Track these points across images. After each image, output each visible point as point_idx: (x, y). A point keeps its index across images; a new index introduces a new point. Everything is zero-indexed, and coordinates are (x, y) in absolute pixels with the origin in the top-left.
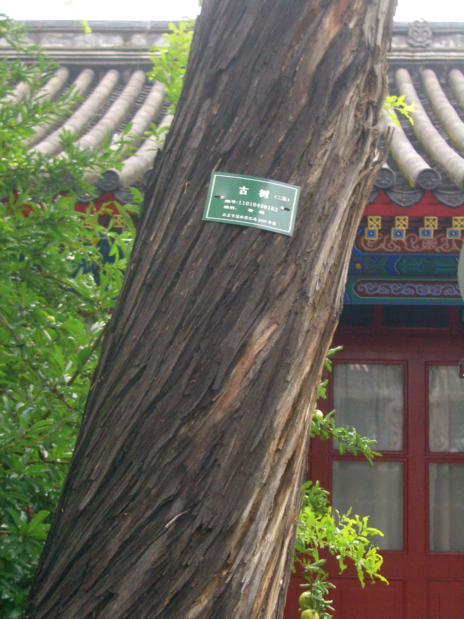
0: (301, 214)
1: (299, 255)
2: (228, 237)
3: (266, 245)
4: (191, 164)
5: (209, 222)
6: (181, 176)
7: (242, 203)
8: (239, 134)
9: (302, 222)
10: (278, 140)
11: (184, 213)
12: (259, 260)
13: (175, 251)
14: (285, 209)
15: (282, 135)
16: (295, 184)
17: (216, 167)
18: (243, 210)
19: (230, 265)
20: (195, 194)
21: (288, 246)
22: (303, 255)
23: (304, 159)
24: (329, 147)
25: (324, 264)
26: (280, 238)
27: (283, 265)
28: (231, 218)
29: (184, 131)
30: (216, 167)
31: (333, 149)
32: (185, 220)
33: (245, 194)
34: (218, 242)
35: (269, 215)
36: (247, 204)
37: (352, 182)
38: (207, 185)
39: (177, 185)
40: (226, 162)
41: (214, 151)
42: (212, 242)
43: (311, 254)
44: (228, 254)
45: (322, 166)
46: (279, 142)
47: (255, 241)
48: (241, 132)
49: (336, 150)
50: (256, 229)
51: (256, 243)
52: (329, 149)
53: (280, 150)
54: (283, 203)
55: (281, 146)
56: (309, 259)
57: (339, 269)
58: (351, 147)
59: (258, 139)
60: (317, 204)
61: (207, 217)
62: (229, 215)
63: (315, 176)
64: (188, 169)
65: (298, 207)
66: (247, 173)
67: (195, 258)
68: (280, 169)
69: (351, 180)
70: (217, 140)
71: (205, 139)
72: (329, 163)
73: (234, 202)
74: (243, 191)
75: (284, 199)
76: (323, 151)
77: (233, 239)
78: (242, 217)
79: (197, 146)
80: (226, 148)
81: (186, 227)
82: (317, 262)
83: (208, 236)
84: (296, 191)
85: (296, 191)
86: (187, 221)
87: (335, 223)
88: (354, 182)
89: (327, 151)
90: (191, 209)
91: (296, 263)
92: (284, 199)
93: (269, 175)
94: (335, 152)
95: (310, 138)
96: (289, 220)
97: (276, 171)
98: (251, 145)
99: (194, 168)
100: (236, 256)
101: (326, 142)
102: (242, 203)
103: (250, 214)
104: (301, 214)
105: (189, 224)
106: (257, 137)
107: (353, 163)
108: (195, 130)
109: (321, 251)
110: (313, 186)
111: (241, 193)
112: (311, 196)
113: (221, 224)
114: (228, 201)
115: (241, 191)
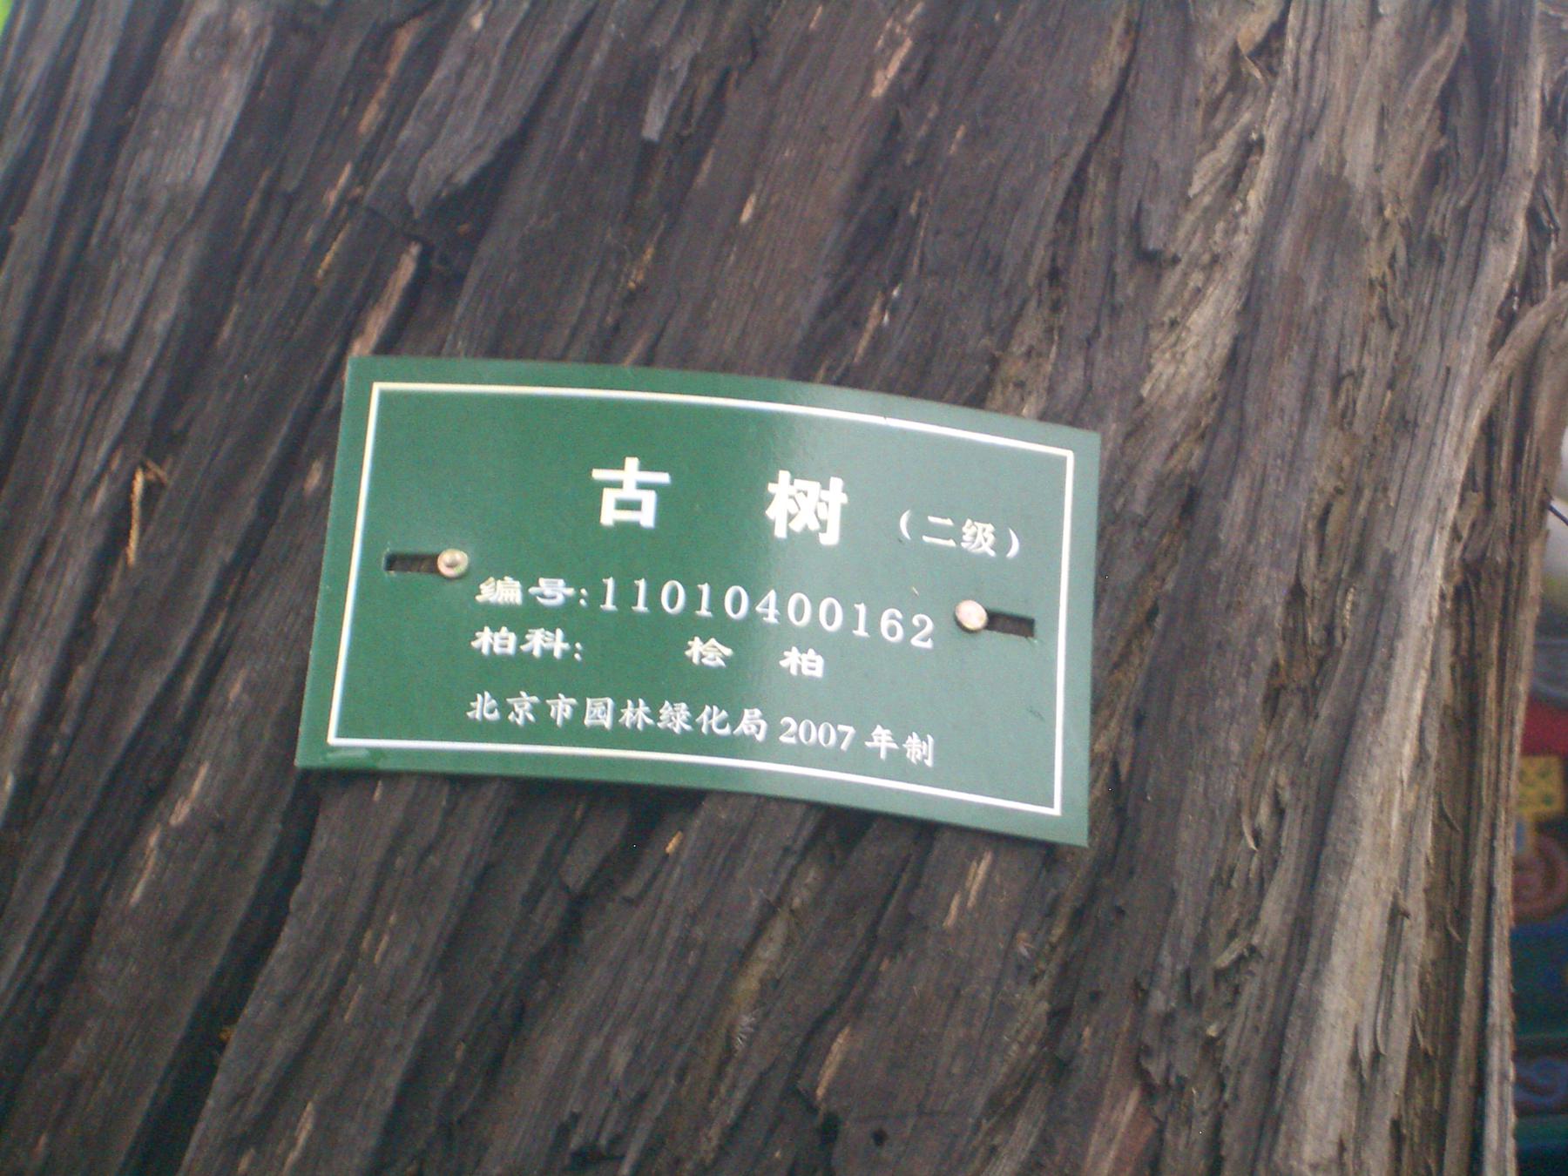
0: (1125, 655)
1: (1159, 1002)
2: (531, 900)
3: (872, 938)
4: (161, 322)
5: (356, 778)
6: (87, 431)
7: (626, 596)
8: (547, 48)
9: (1139, 721)
10: (868, 83)
11: (135, 718)
12: (828, 1072)
13: (80, 1051)
14: (995, 620)
15: (894, 43)
16: (1043, 417)
17: (376, 324)
18: (636, 657)
19: (575, 1142)
20: (221, 553)
21: (1058, 931)
22: (1191, 1000)
23: (1093, 211)
24: (1270, 120)
25: (1354, 1060)
26: (980, 871)
27: (1036, 1100)
28: (542, 728)
29: (93, 73)
30: (376, 324)
31: (1299, 137)
32: (149, 775)
33: (646, 517)
34: (456, 942)
35: (863, 679)
36: (673, 597)
37: (1458, 392)
38: (314, 480)
39: (63, 495)
40: (457, 280)
41: (349, 202)
42: (396, 950)
43: (1251, 989)
44: (551, 1046)
45: (1235, 272)
46: (878, 91)
47: (770, 911)
48: (565, 28)
49: (1324, 138)
50: (764, 807)
51: (779, 929)
52: (1271, 134)
53: (891, 150)
54: (967, 574)
55: (896, 126)
56: (1238, 1036)
57: (1460, 1094)
58: (1416, 132)
59: (705, 85)
60: (1244, 569)
61: (337, 739)
62: (523, 708)
63: (1188, 352)
64: (144, 361)
65: (1101, 591)
66: (638, 348)
67: (253, 1109)
68: (912, 299)
69: (1448, 375)
70: (371, 117)
71: (272, 116)
72: (1286, 239)
73: (554, 591)
74: (630, 493)
75: (979, 537)
76: (1224, 152)
77: (579, 908)
78: (636, 715)
79: (204, 175)
80: (453, 154)
81: (153, 840)
82: (1307, 1054)
83: (357, 904)
84: (1069, 461)
85: (1069, 461)
86: (159, 792)
87: (1393, 717)
88: (1472, 393)
89: (1250, 148)
90: (190, 682)
91: (1143, 1074)
92: (979, 537)
93: (819, 358)
94: (1316, 156)
95: (1116, 56)
96: (1044, 716)
97: (877, 318)
98: (653, 127)
99: (192, 353)
100: (620, 1059)
101: (1237, 83)
102: (626, 596)
103: (699, 687)
104: (1125, 655)
105: (181, 813)
106: (694, 65)
107: (1433, 250)
108: (179, 52)
109: (1324, 955)
110: (1192, 426)
111: (609, 515)
112: (1189, 500)
113: (462, 784)
114: (503, 591)
115: (610, 497)
